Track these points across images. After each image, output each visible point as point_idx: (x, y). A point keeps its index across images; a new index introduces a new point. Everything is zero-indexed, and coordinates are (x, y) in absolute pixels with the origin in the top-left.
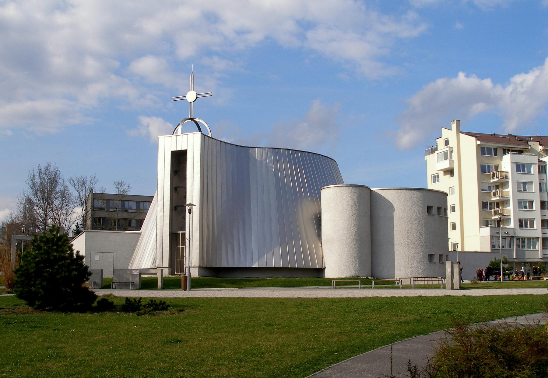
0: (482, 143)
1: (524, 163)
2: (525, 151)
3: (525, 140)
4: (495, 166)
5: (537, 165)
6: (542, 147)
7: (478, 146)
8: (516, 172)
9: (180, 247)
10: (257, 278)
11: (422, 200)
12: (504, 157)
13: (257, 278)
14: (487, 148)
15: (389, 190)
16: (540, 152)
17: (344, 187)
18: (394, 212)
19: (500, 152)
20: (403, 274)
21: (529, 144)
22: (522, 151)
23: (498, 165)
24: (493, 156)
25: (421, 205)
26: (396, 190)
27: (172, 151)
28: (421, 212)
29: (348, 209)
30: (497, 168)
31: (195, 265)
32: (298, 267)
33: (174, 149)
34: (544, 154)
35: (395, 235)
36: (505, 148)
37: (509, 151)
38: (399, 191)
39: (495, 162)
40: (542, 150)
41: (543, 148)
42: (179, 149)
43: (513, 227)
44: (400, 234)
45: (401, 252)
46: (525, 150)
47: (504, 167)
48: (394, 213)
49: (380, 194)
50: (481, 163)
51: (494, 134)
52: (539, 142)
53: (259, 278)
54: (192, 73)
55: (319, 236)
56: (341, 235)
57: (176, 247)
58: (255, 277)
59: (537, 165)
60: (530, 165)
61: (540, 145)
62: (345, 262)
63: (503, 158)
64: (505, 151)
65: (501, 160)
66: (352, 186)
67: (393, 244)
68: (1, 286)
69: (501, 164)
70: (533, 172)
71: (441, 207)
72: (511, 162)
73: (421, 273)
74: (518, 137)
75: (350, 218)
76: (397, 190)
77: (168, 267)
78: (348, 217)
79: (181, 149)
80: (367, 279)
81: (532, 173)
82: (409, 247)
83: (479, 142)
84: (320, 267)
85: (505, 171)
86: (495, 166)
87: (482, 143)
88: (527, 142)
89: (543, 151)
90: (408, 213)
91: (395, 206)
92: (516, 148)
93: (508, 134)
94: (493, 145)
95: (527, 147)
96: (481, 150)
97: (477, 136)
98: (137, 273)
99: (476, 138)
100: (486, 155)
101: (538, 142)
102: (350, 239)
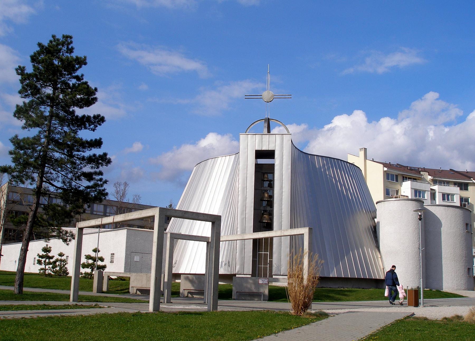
0: (388, 170)
1: (420, 190)
2: (418, 179)
3: (418, 171)
4: (396, 190)
5: (430, 192)
6: (432, 177)
7: (385, 172)
8: (415, 197)
9: (263, 253)
10: (330, 288)
11: (462, 218)
12: (403, 183)
13: (330, 288)
14: (391, 174)
15: (437, 207)
16: (429, 181)
17: (409, 201)
18: (441, 226)
19: (400, 178)
20: (451, 286)
21: (421, 174)
22: (415, 179)
23: (399, 190)
24: (395, 181)
25: (462, 222)
26: (439, 207)
27: (257, 150)
28: (462, 229)
29: (412, 223)
30: (397, 192)
31: (284, 274)
32: (351, 277)
33: (258, 149)
34: (432, 183)
35: (442, 249)
36: (404, 176)
37: (411, 178)
38: (446, 208)
39: (397, 187)
40: (431, 180)
41: (432, 178)
42: (265, 148)
43: (174, 239)
44: (448, 248)
45: (449, 265)
46: (418, 178)
47: (404, 192)
48: (442, 228)
49: (430, 210)
50: (386, 187)
51: (390, 163)
52: (428, 172)
53: (332, 288)
54: (268, 72)
55: (378, 247)
56: (406, 248)
57: (258, 253)
58: (328, 287)
59: (430, 192)
60: (424, 191)
61: (429, 175)
62: (410, 274)
63: (402, 184)
64: (405, 178)
65: (401, 186)
66: (416, 200)
67: (441, 258)
68: (1, 286)
69: (401, 188)
70: (427, 198)
71: (468, 223)
72: (411, 188)
73: (464, 286)
74: (410, 167)
75: (414, 231)
76: (444, 207)
77: (251, 274)
78: (413, 231)
79: (261, 149)
80: (430, 292)
81: (426, 198)
82: (455, 261)
83: (386, 169)
84: (383, 279)
85: (406, 195)
86: (396, 190)
87: (388, 170)
88: (420, 172)
89: (431, 181)
90: (453, 229)
91: (443, 222)
92: (411, 176)
93: (397, 164)
94: (395, 172)
95: (420, 176)
96: (388, 176)
97: (385, 165)
98: (265, 282)
99: (383, 165)
100: (390, 180)
101: (428, 173)
102: (414, 252)
